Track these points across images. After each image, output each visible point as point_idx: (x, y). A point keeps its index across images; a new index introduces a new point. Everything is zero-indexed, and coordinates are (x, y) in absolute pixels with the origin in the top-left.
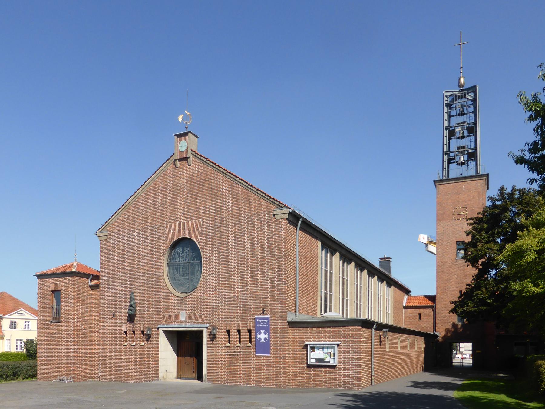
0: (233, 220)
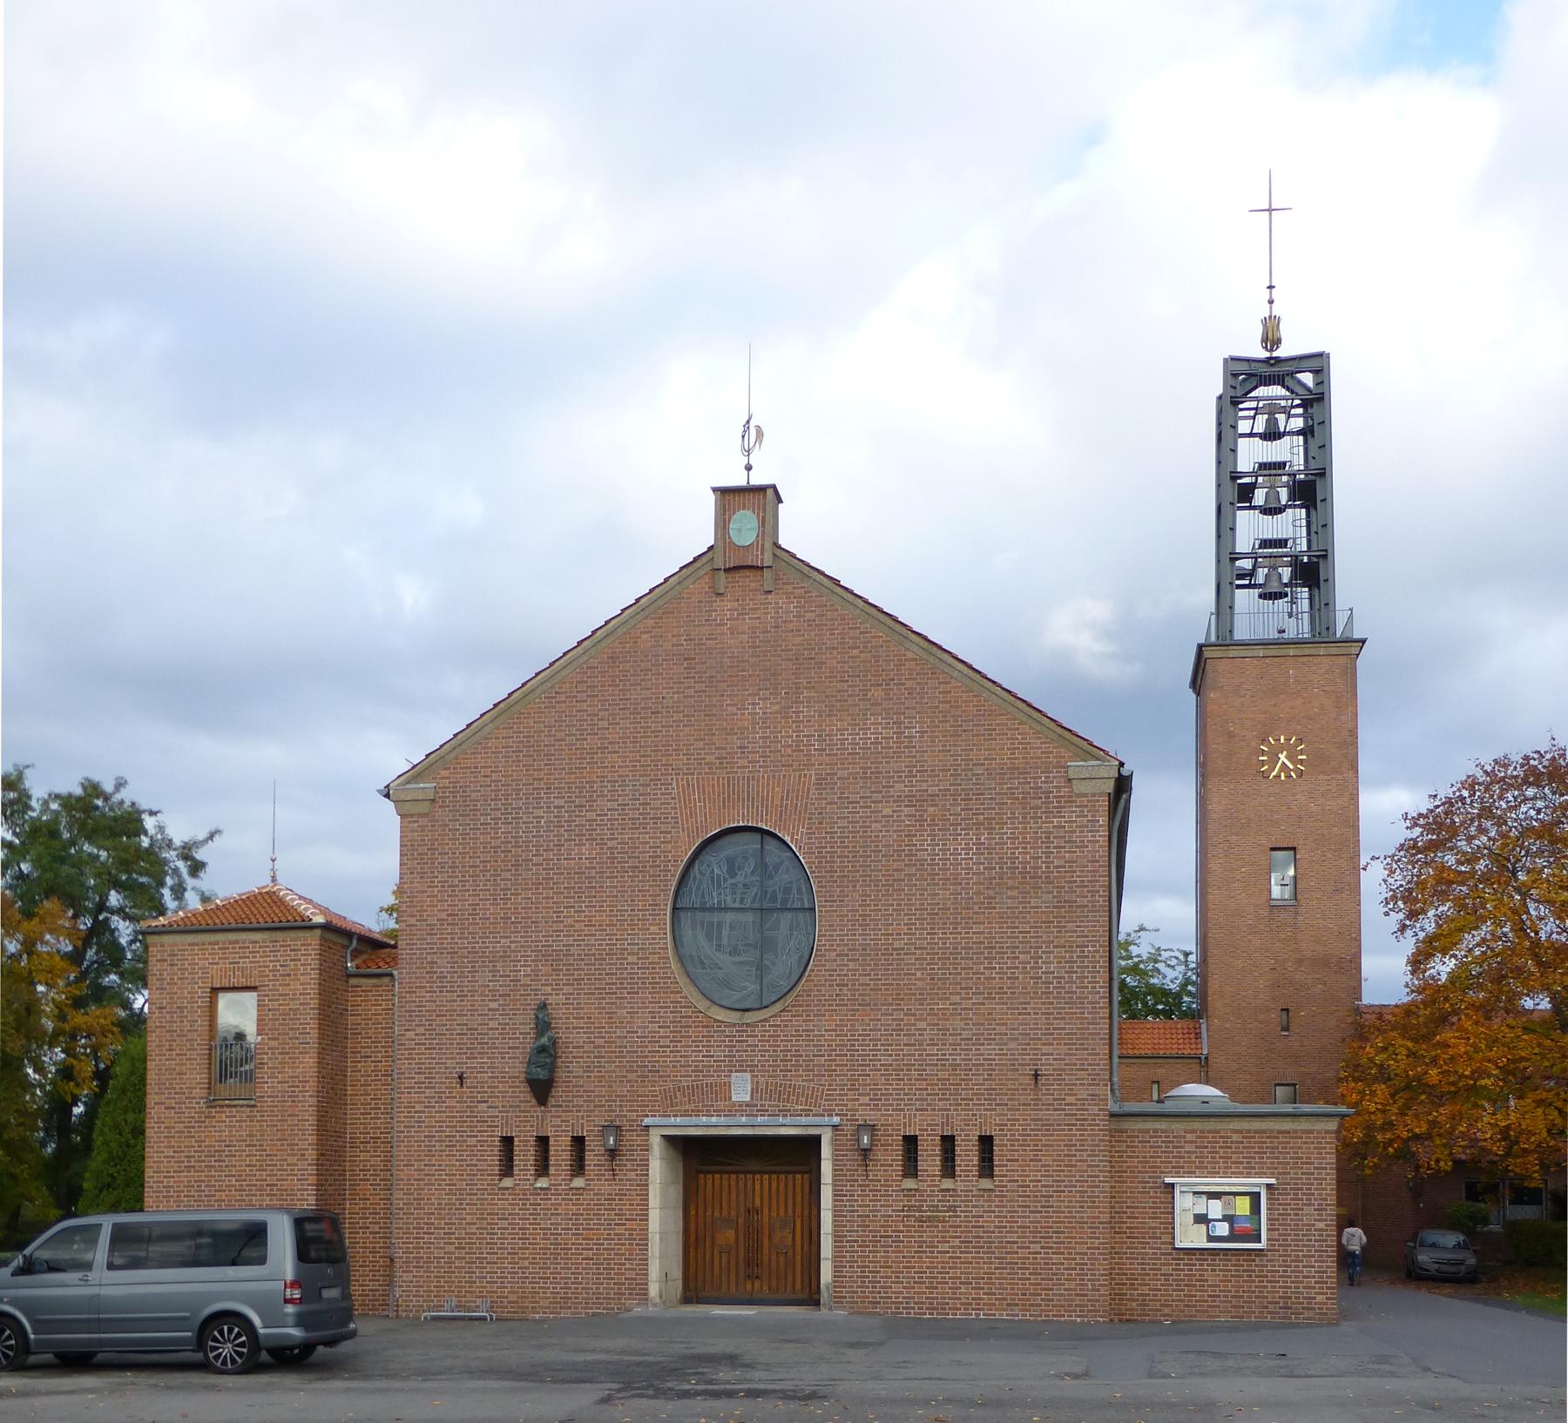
0: (925, 784)
